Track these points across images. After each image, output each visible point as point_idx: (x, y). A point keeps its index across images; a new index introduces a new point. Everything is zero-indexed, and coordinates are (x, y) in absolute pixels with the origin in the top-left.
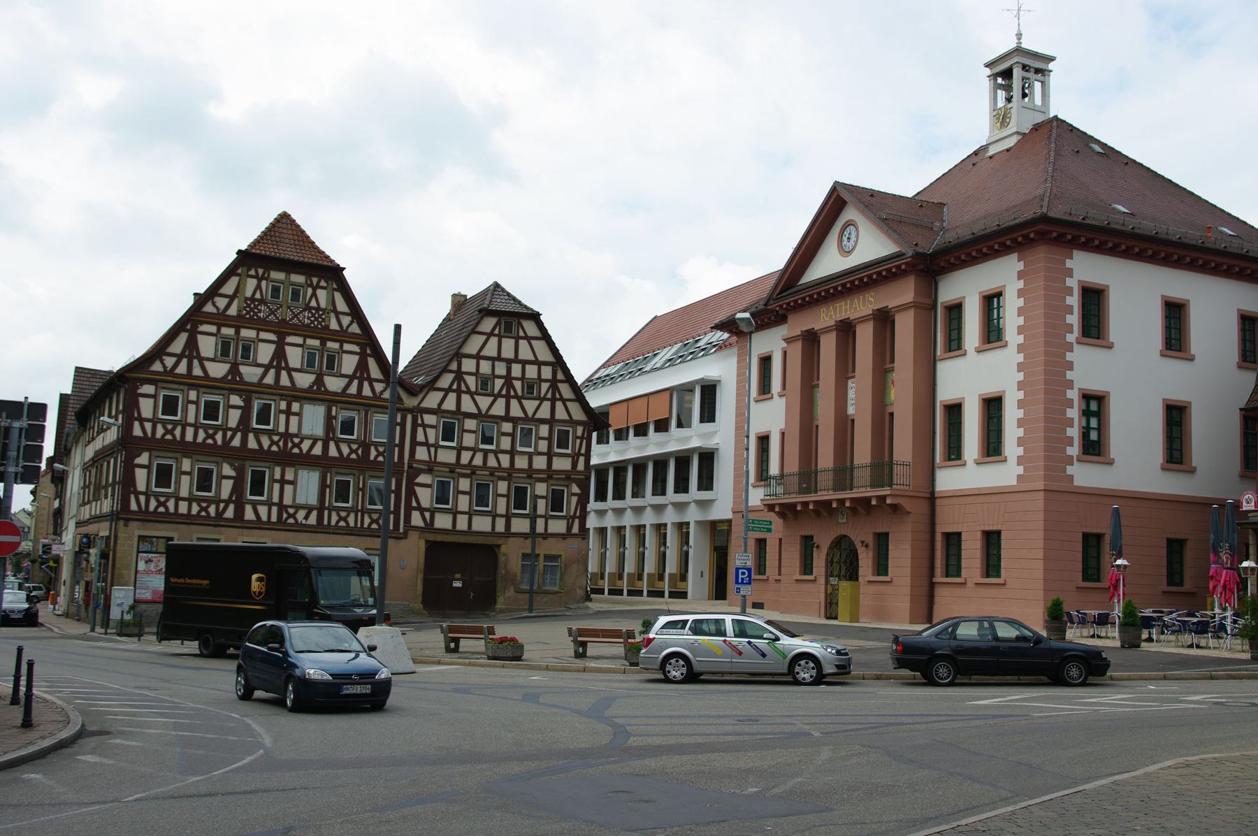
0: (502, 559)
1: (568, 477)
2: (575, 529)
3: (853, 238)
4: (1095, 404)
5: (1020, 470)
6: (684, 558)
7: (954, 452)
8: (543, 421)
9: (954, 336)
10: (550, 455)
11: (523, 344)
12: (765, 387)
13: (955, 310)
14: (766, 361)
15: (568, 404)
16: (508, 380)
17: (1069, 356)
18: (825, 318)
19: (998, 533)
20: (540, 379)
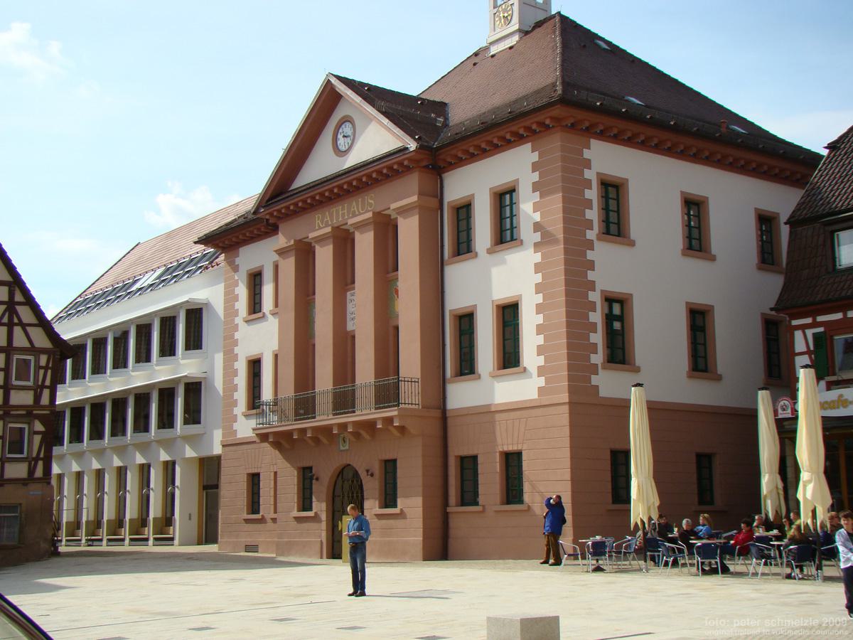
1: (29, 414)
2: (39, 472)
4: (618, 310)
5: (541, 382)
6: (169, 500)
7: (467, 366)
9: (463, 236)
12: (255, 305)
13: (464, 211)
15: (29, 329)
17: (590, 255)
18: (319, 226)
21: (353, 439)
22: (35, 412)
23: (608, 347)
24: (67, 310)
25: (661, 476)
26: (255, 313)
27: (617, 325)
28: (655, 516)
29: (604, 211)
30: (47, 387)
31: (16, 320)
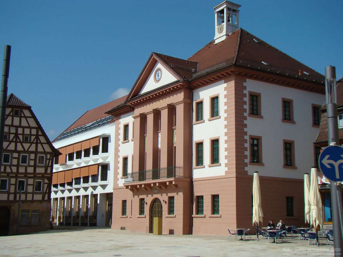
0: (12, 212)
1: (43, 176)
2: (46, 198)
3: (160, 75)
7: (200, 162)
8: (32, 152)
10: (35, 167)
11: (23, 120)
12: (126, 137)
13: (200, 104)
14: (126, 127)
15: (43, 145)
16: (16, 135)
17: (245, 122)
18: (147, 109)
19: (202, 197)
20: (31, 135)
21: (159, 189)
22: (45, 176)
23: (252, 156)
24: (60, 136)
25: (263, 205)
26: (126, 140)
27: (255, 148)
28: (262, 221)
29: (251, 105)
30: (50, 166)
31: (39, 142)
